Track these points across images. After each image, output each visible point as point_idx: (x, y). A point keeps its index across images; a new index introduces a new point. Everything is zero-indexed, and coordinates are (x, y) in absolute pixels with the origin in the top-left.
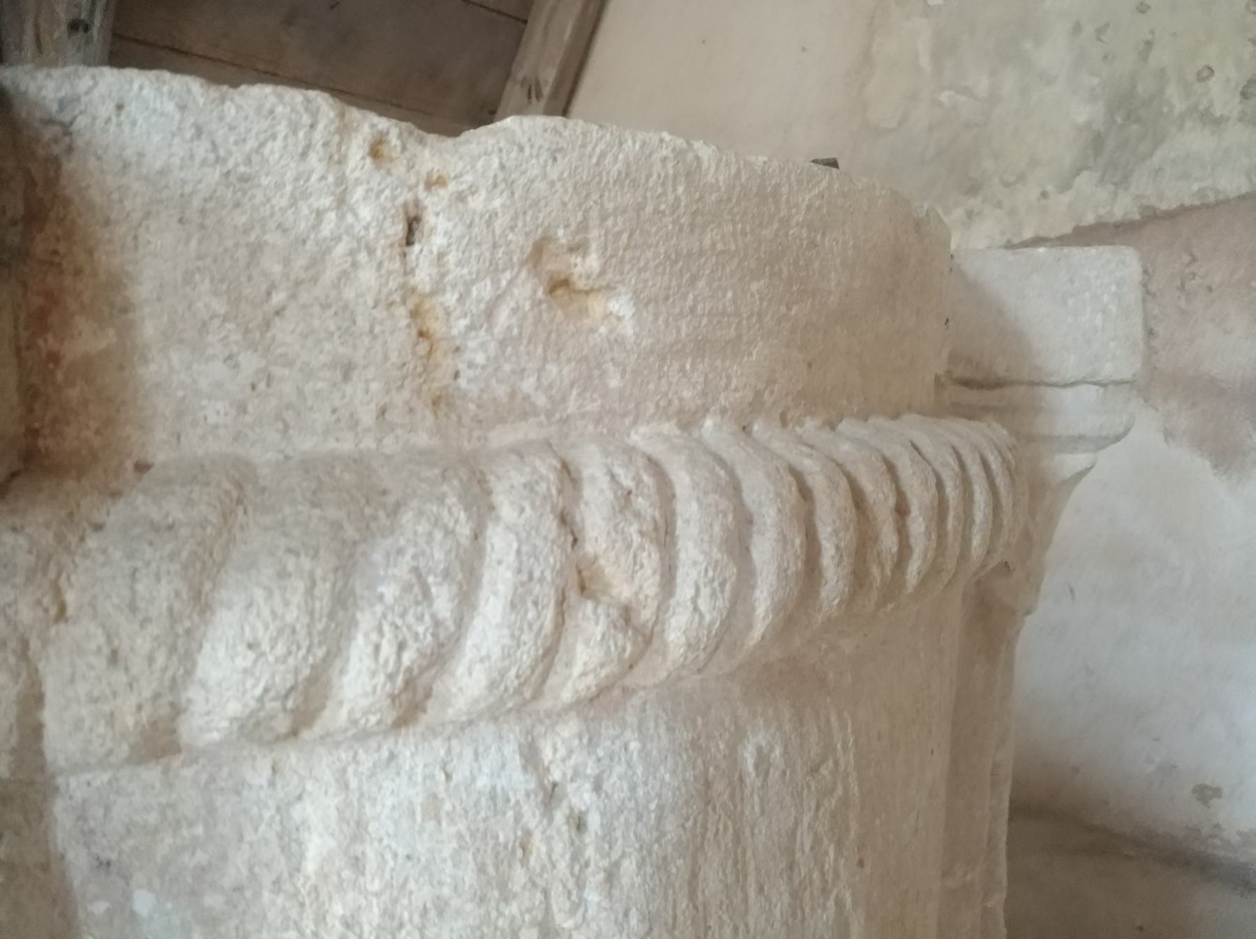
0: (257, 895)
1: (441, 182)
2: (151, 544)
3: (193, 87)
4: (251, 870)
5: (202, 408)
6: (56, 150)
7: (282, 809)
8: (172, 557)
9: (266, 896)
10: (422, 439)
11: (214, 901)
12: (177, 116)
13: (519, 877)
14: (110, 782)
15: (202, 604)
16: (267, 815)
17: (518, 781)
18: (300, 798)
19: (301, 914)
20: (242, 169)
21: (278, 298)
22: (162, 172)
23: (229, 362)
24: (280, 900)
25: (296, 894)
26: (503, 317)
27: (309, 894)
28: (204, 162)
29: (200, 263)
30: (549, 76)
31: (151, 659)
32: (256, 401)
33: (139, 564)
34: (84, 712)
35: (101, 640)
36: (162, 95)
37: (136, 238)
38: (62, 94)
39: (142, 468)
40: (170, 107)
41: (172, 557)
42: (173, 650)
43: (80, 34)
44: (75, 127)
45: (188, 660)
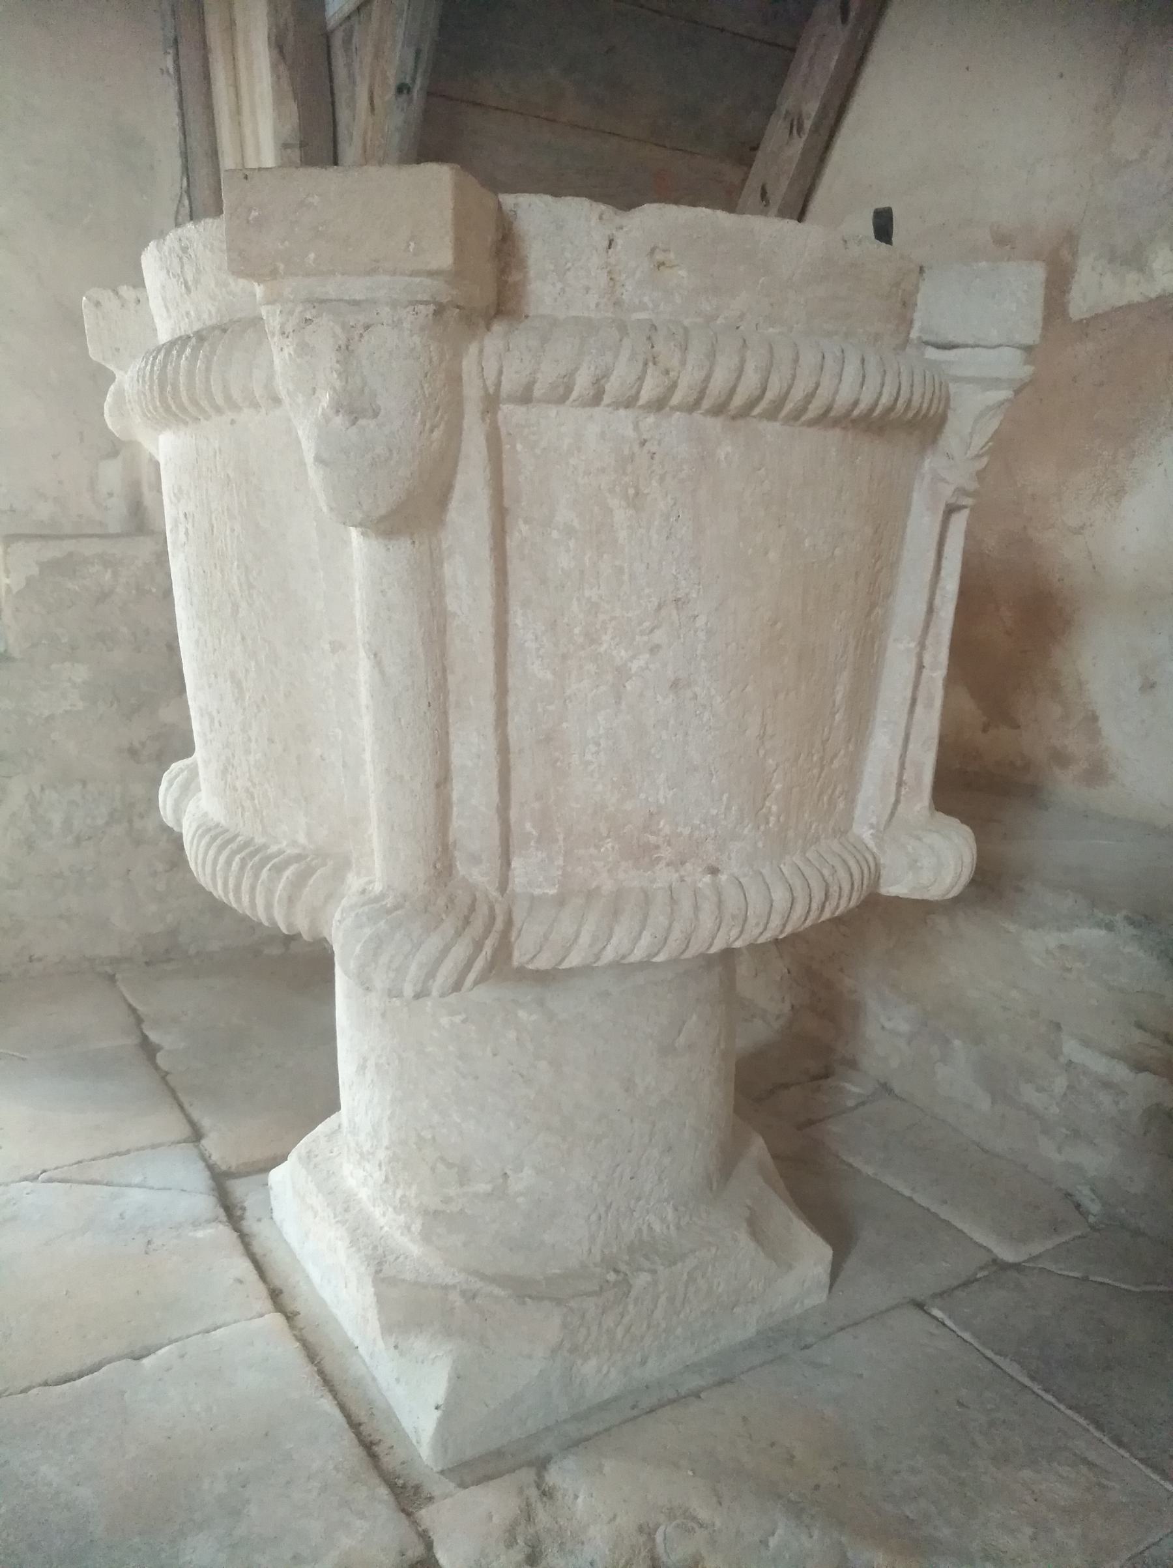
1: (621, 228)
3: (548, 198)
10: (609, 315)
11: (538, 451)
13: (629, 468)
17: (630, 432)
20: (561, 223)
21: (569, 265)
26: (638, 275)
30: (812, 108)
39: (527, 317)
43: (404, 96)
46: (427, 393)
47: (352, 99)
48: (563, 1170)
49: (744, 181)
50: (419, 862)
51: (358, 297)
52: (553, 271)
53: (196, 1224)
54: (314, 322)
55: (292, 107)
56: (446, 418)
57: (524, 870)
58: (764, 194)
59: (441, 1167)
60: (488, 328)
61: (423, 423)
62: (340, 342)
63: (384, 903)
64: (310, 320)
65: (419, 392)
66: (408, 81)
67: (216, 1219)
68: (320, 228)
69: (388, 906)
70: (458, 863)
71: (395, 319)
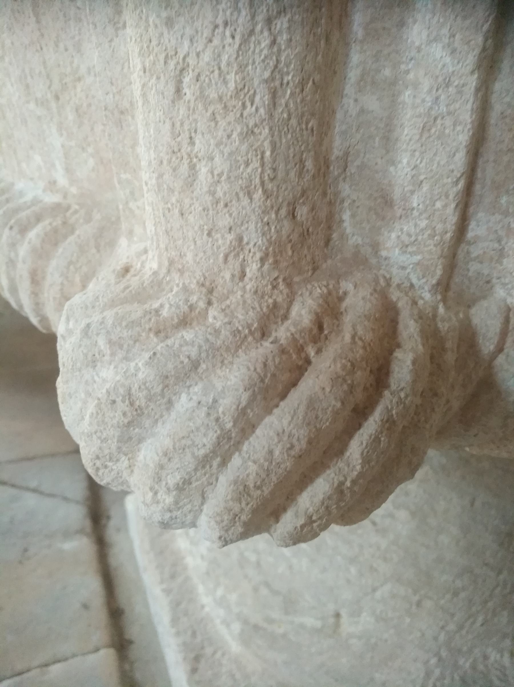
48: (408, 620)
50: (250, 195)
53: (67, 535)
57: (496, 245)
59: (264, 591)
63: (156, 305)
67: (81, 531)
69: (165, 313)
70: (346, 216)
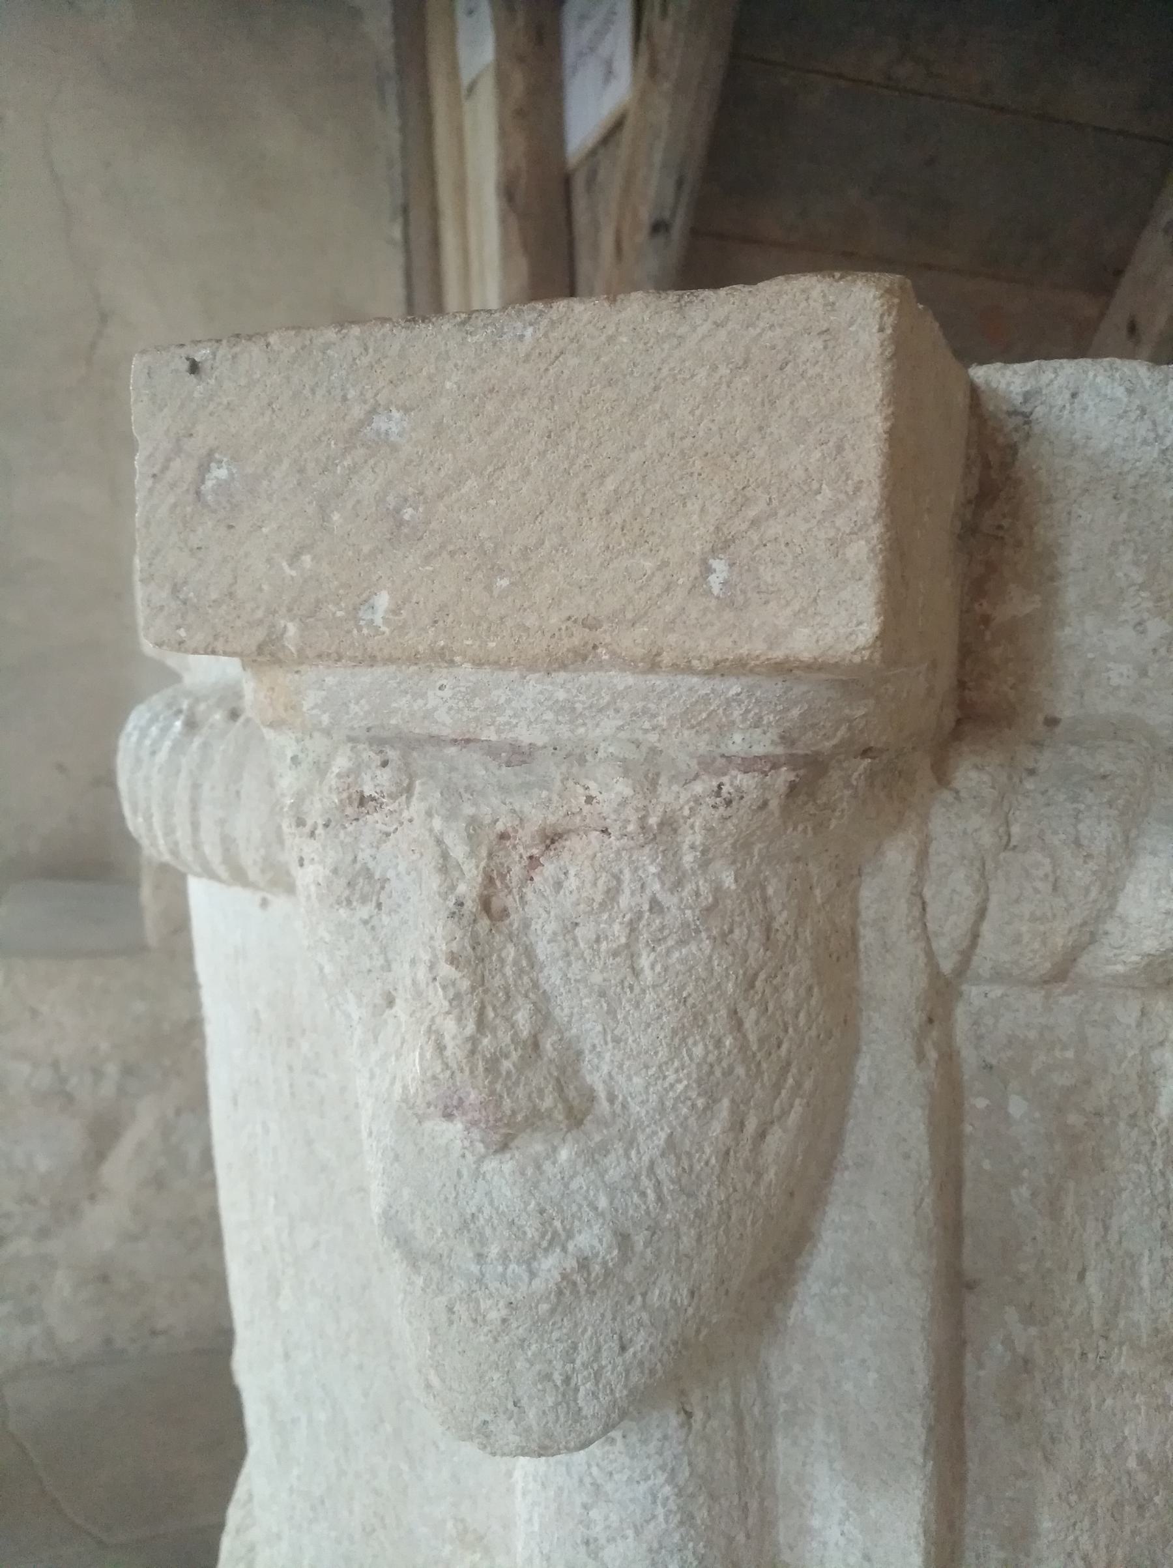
0: (1114, 1124)
2: (1091, 790)
4: (1111, 1099)
5: (1108, 670)
6: (1016, 437)
7: (1145, 1051)
8: (1110, 803)
9: (1122, 1126)
12: (1125, 400)
14: (1002, 996)
15: (1129, 848)
16: (1130, 1054)
18: (1162, 1044)
19: (1152, 1150)
22: (1105, 453)
23: (1138, 628)
24: (1135, 1133)
25: (1148, 1132)
27: (1161, 1136)
28: (1145, 442)
29: (1127, 536)
31: (1087, 890)
32: (1156, 665)
33: (1082, 807)
34: (1024, 929)
35: (1048, 868)
36: (1113, 380)
37: (1069, 513)
38: (1028, 388)
39: (1052, 722)
40: (1120, 392)
41: (1110, 803)
42: (1103, 887)
44: (1033, 417)
45: (1113, 894)
46: (752, 1037)
47: (595, 247)
49: (1102, 315)
51: (525, 735)
52: (1142, 587)
54: (386, 809)
55: (522, 264)
56: (808, 1084)
58: (1133, 328)
60: (942, 777)
61: (738, 1125)
62: (462, 888)
64: (373, 799)
65: (728, 1042)
66: (667, 214)
68: (408, 513)
71: (653, 821)
